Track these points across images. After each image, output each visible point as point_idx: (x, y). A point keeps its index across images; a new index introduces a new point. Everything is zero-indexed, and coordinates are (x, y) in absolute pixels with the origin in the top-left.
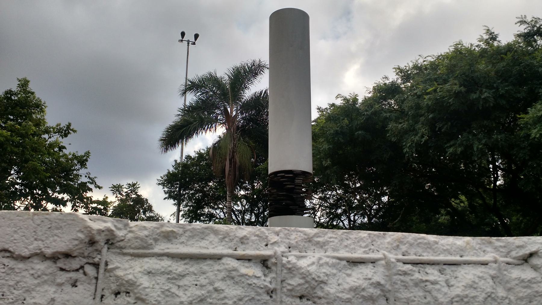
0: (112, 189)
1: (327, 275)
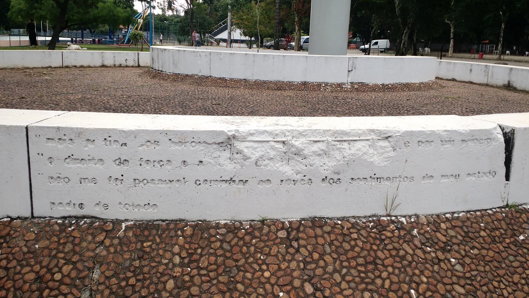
1: (305, 147)
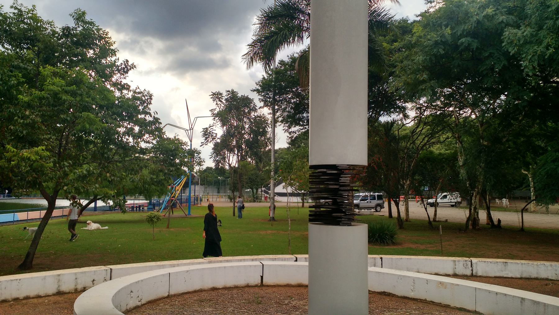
0: (211, 96)
